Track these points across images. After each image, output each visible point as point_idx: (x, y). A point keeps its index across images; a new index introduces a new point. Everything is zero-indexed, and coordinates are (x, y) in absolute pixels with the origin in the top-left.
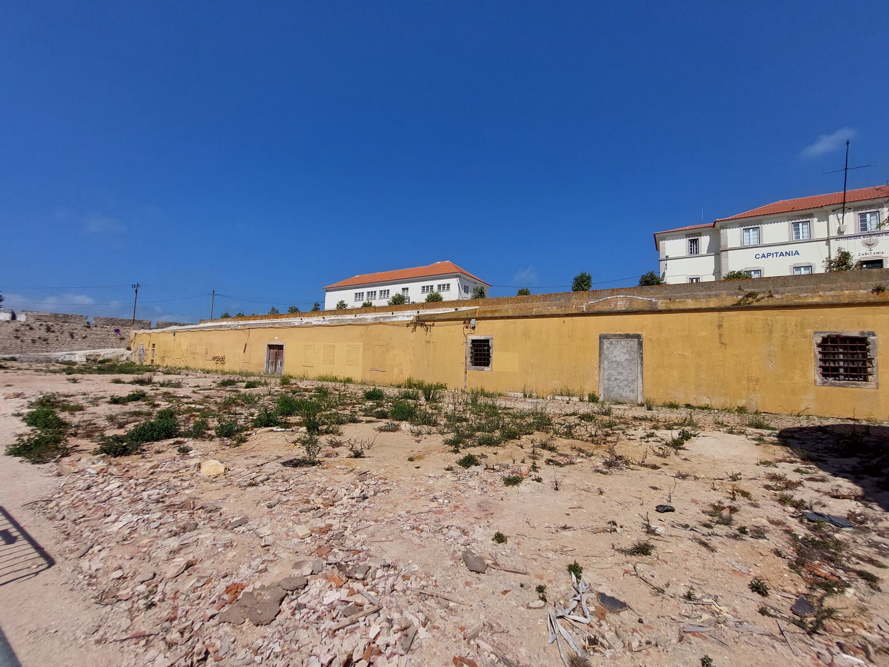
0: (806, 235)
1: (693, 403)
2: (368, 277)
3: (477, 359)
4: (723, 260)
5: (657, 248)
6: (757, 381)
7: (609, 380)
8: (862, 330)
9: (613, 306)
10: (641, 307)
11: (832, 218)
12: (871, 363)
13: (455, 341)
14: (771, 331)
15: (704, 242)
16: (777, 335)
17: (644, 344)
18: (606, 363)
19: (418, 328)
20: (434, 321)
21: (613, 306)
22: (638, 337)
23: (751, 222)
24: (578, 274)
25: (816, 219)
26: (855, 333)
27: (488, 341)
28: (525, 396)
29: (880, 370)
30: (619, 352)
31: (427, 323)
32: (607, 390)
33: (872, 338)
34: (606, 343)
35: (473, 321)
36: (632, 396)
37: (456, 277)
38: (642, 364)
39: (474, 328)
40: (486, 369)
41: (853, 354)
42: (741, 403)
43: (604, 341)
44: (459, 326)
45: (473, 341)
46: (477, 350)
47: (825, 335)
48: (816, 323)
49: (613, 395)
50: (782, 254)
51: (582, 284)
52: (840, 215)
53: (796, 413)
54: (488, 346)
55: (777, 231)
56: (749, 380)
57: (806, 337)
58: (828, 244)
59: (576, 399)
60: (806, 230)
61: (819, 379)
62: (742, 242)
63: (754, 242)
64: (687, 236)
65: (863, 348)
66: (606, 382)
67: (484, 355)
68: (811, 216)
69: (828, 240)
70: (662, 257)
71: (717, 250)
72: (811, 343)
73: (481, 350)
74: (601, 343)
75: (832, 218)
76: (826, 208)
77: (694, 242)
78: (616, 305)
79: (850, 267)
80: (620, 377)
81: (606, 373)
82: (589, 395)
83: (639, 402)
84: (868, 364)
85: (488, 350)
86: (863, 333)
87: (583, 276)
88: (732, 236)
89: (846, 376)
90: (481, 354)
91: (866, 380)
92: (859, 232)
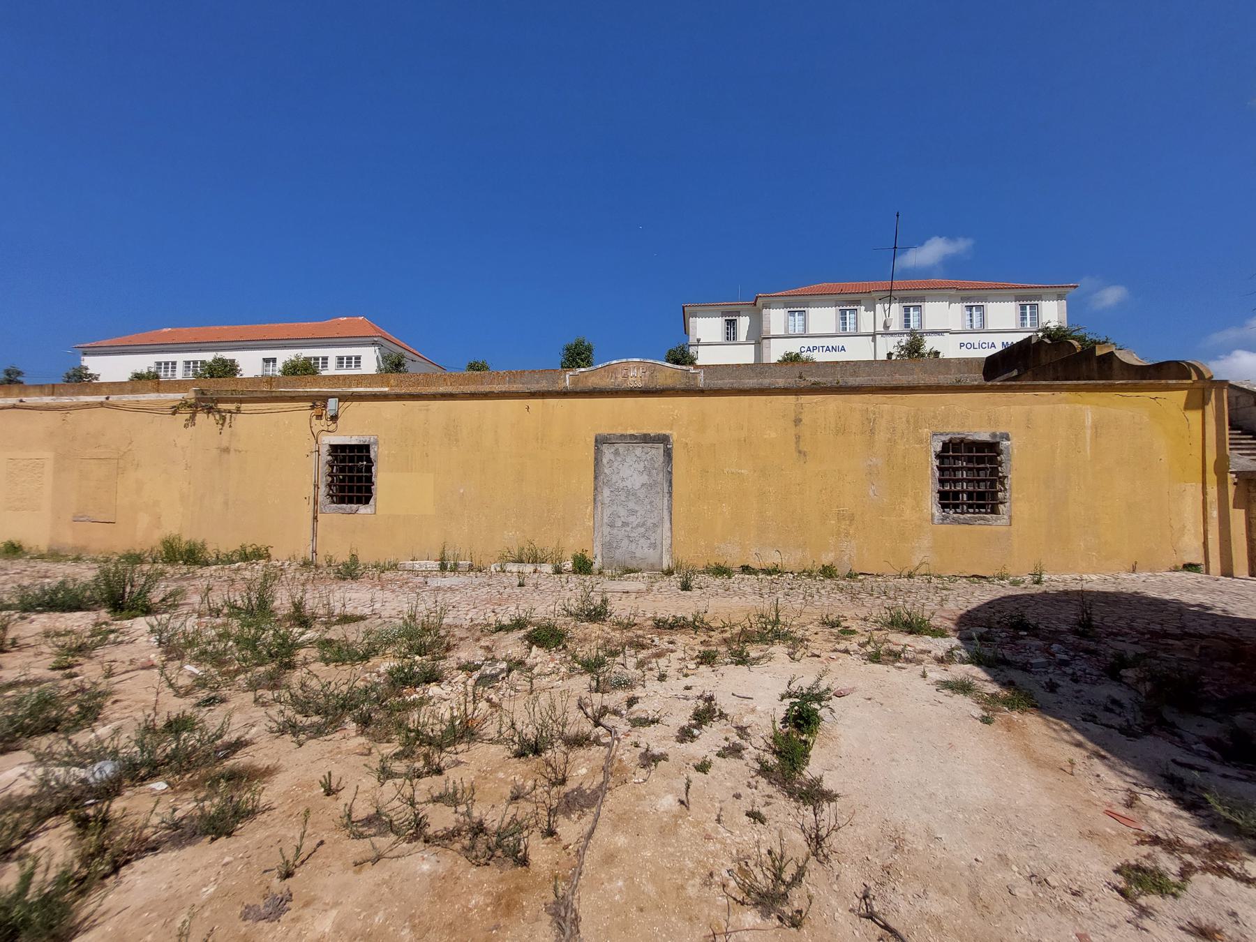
0: (853, 326)
1: (754, 564)
2: (188, 333)
3: (342, 489)
4: (765, 350)
5: (686, 331)
6: (852, 518)
7: (612, 526)
8: (993, 430)
9: (620, 378)
10: (669, 383)
11: (879, 307)
12: (1002, 484)
13: (288, 447)
14: (872, 431)
15: (743, 323)
16: (881, 436)
17: (674, 455)
18: (606, 492)
19: (201, 417)
20: (241, 401)
21: (620, 378)
22: (664, 439)
23: (797, 305)
24: (572, 341)
25: (863, 308)
26: (984, 436)
27: (365, 448)
28: (443, 567)
29: (1014, 495)
30: (631, 470)
31: (222, 406)
32: (608, 546)
33: (1005, 443)
34: (608, 452)
35: (332, 403)
36: (652, 555)
37: (374, 344)
38: (670, 493)
39: (334, 418)
40: (363, 509)
41: (979, 470)
42: (827, 559)
43: (605, 448)
44: (298, 417)
45: (334, 448)
46: (342, 470)
47: (946, 438)
48: (934, 417)
49: (618, 554)
50: (828, 349)
51: (577, 356)
52: (887, 306)
53: (905, 573)
54: (369, 460)
55: (823, 318)
56: (840, 517)
57: (921, 442)
58: (874, 340)
59: (547, 568)
60: (853, 321)
61: (936, 511)
62: (787, 329)
63: (799, 330)
64: (723, 314)
65: (992, 460)
66: (607, 530)
67: (360, 479)
68: (858, 303)
69: (874, 335)
70: (692, 340)
71: (758, 338)
72: (927, 451)
73: (351, 469)
74: (598, 452)
75: (879, 307)
76: (874, 295)
77: (731, 324)
78: (626, 377)
79: (923, 355)
80: (632, 519)
81: (607, 512)
82: (575, 558)
83: (665, 567)
84: (999, 486)
85: (369, 469)
86: (994, 435)
87: (579, 344)
88: (776, 319)
89: (970, 506)
90: (351, 476)
91: (994, 511)
92: (902, 329)
